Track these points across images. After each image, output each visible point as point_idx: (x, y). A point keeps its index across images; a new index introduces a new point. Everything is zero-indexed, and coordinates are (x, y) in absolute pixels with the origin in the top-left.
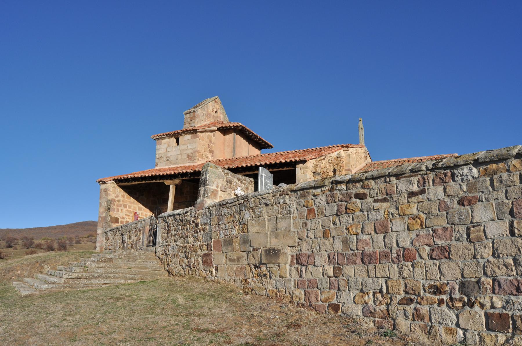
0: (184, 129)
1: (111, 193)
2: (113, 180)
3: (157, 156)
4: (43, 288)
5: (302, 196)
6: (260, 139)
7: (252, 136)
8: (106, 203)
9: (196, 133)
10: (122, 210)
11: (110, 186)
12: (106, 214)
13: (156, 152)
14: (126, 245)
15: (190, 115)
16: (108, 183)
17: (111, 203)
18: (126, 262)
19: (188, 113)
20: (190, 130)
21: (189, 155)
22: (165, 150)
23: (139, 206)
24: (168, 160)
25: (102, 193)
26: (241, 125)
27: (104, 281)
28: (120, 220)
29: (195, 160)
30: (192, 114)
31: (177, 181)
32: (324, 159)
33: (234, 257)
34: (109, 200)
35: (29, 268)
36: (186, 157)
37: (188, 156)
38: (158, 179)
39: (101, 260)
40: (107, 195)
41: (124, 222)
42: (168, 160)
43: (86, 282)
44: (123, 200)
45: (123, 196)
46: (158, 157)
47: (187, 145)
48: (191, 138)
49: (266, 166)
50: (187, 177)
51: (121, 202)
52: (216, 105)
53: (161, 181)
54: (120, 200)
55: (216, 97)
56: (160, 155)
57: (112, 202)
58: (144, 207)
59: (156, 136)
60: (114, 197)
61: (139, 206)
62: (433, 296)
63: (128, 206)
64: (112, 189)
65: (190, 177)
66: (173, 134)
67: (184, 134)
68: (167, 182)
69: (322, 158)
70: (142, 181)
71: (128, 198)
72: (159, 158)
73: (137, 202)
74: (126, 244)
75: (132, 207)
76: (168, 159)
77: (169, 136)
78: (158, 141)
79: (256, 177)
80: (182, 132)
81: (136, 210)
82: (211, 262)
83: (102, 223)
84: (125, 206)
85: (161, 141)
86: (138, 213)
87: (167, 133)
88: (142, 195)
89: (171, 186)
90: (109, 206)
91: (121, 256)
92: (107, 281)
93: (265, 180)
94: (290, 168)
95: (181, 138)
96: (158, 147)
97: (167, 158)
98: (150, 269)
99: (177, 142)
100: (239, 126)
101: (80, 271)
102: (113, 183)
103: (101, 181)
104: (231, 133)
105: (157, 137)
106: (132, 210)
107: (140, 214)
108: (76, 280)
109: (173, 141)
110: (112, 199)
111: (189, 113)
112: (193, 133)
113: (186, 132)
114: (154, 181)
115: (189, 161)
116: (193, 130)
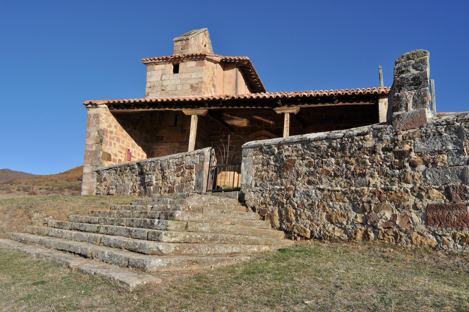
0: (186, 54)
1: (104, 121)
2: (106, 104)
3: (148, 85)
4: (153, 267)
6: (259, 80)
7: (253, 75)
8: (97, 133)
9: (203, 59)
10: (115, 144)
11: (102, 111)
12: (96, 147)
13: (146, 79)
14: (152, 189)
15: (182, 43)
16: (100, 107)
17: (103, 133)
18: (219, 213)
19: (179, 41)
20: (197, 55)
21: (193, 85)
22: (160, 78)
23: (132, 142)
24: (163, 90)
25: (90, 119)
26: (248, 60)
27: (232, 248)
28: (113, 157)
29: (201, 92)
30: (184, 42)
31: (202, 111)
34: (101, 130)
35: (7, 216)
36: (189, 87)
37: (192, 87)
38: (174, 106)
39: (187, 209)
40: (98, 122)
41: (116, 160)
42: (163, 90)
43: (208, 250)
44: (116, 132)
45: (116, 127)
46: (149, 86)
47: (190, 74)
48: (197, 66)
50: (217, 106)
51: (114, 134)
53: (178, 109)
54: (113, 131)
55: (207, 29)
57: (105, 133)
58: (136, 145)
59: (148, 59)
60: (106, 127)
61: (132, 142)
63: (121, 140)
64: (104, 116)
65: (222, 106)
66: (172, 59)
67: (186, 60)
68: (186, 111)
70: (149, 108)
71: (121, 131)
72: (150, 87)
73: (130, 137)
74: (152, 187)
75: (125, 143)
76: (164, 89)
77: (166, 60)
78: (149, 67)
80: (185, 57)
81: (129, 147)
83: (91, 159)
84: (118, 140)
85: (154, 67)
86: (131, 151)
87: (164, 57)
88: (135, 129)
89: (193, 117)
90: (102, 137)
91: (206, 204)
92: (235, 249)
94: (368, 103)
95: (181, 66)
96: (149, 73)
97: (163, 88)
98: (255, 225)
99: (176, 70)
100: (246, 60)
101: (176, 228)
102: (105, 107)
103: (91, 103)
104: (233, 69)
105: (150, 61)
106: (125, 146)
107: (132, 152)
108: (193, 247)
109: (171, 68)
110: (105, 129)
111: (180, 40)
112: (199, 60)
113: (190, 58)
114: (167, 109)
115: (194, 93)
116: (201, 55)
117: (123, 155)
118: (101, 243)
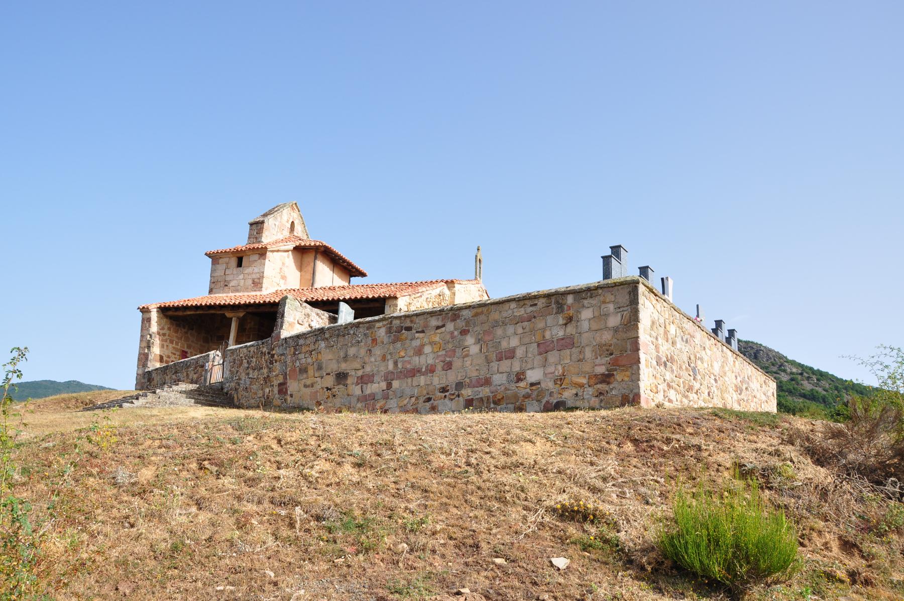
5: (368, 329)
10: (167, 346)
32: (421, 296)
33: (309, 382)
36: (250, 282)
49: (344, 300)
52: (292, 214)
56: (216, 278)
62: (442, 394)
69: (419, 294)
79: (336, 312)
82: (287, 390)
88: (192, 329)
93: (345, 316)
97: (226, 283)
99: (240, 264)
117: (176, 356)
118: (42, 426)
